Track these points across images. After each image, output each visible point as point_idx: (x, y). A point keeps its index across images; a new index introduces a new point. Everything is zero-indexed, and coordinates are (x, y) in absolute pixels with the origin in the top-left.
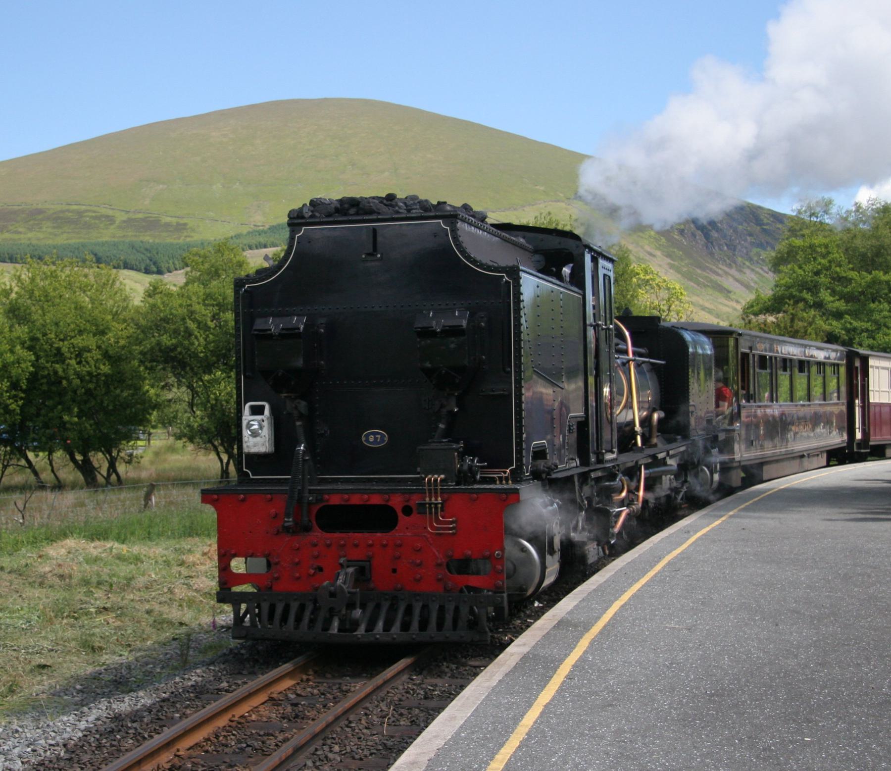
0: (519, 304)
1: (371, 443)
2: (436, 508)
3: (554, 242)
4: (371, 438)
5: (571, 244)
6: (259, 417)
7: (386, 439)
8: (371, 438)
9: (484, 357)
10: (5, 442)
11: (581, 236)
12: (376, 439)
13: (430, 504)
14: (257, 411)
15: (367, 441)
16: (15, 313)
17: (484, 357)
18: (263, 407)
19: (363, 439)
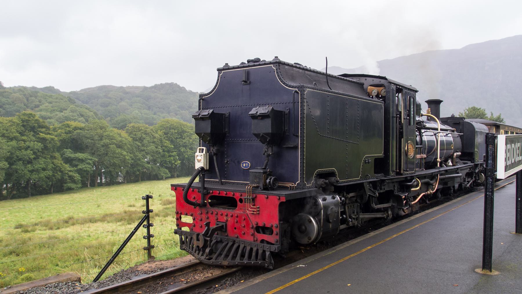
7: (250, 165)
12: (246, 165)
13: (248, 199)
15: (243, 166)
18: (203, 150)
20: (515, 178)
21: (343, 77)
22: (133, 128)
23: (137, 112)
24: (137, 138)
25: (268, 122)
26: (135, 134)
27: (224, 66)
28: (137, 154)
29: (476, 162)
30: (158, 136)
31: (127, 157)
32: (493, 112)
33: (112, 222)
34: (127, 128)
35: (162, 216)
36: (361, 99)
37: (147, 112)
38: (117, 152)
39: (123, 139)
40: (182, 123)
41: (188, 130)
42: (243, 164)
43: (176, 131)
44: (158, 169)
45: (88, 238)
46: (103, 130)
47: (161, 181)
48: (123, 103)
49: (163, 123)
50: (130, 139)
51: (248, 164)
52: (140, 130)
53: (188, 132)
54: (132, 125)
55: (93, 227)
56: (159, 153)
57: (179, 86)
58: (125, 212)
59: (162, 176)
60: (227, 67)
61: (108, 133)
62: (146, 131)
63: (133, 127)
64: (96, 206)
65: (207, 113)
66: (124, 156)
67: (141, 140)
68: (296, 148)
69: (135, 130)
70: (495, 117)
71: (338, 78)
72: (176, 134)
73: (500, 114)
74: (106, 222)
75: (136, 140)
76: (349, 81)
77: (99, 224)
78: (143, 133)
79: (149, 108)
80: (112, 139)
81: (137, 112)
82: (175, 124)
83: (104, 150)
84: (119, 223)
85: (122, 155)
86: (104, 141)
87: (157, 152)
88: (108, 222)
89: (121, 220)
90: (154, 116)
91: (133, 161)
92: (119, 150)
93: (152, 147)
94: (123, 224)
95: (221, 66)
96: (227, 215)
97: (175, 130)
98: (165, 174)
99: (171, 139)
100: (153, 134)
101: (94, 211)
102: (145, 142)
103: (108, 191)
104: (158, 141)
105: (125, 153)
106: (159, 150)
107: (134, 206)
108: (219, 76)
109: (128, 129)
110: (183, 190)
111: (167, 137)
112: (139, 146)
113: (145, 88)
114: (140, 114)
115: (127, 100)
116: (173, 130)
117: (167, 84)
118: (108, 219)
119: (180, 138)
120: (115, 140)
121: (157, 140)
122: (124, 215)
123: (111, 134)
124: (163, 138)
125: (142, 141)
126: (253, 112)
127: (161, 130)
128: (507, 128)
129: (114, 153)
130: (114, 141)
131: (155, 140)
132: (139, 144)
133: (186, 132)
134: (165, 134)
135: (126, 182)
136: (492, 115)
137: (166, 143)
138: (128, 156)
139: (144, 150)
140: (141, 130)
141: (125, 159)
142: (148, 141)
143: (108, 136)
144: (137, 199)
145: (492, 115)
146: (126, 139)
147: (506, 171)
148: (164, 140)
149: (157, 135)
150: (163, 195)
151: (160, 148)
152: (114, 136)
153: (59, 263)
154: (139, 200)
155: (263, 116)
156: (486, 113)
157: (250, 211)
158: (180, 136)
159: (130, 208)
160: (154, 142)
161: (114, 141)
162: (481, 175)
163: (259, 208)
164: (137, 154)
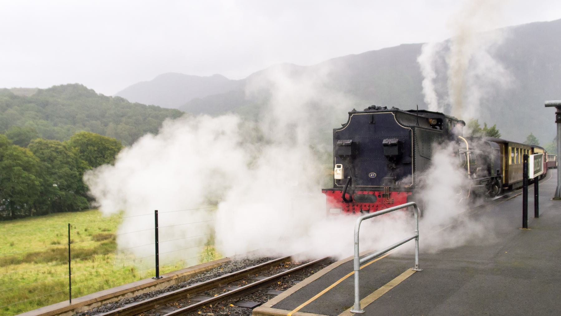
0: (414, 135)
1: (372, 177)
2: (387, 195)
3: (439, 117)
4: (372, 175)
5: (442, 117)
6: (339, 169)
7: (376, 175)
8: (372, 175)
9: (506, 252)
10: (249, 315)
11: (443, 113)
12: (373, 175)
13: (386, 195)
14: (339, 167)
15: (370, 176)
16: (2, 280)
17: (506, 252)
18: (340, 166)
19: (369, 175)
20: (522, 191)
21: (410, 113)
22: (40, 145)
23: (31, 122)
24: (46, 158)
25: (396, 148)
26: (42, 152)
27: (352, 111)
28: (48, 177)
29: (493, 176)
30: (73, 155)
31: (37, 183)
32: (487, 123)
33: (40, 262)
34: (30, 144)
35: (101, 253)
36: (429, 129)
37: (45, 122)
38: (23, 175)
39: (30, 159)
40: (103, 138)
41: (111, 147)
42: (370, 174)
43: (96, 149)
44: (74, 197)
45: (22, 280)
46: (4, 147)
47: (78, 213)
48: (10, 111)
49: (78, 138)
50: (38, 160)
51: (375, 175)
52: (48, 148)
53: (112, 149)
54: (38, 140)
55: (22, 268)
56: (76, 176)
57: (85, 89)
58: (53, 250)
59: (79, 206)
60: (354, 112)
61: (11, 151)
62: (57, 148)
63: (40, 143)
64: (9, 245)
65: (349, 143)
66: (33, 181)
67: (51, 159)
68: (411, 163)
69: (43, 148)
70: (489, 129)
71: (405, 113)
72: (96, 152)
73: (495, 125)
74: (33, 263)
75: (44, 161)
76: (412, 115)
77: (25, 266)
78: (53, 151)
79: (47, 117)
80: (15, 160)
81: (31, 122)
82: (94, 139)
83: (5, 174)
84: (50, 264)
85: (30, 179)
86: (6, 162)
87: (71, 175)
88: (36, 263)
89: (51, 260)
90: (56, 128)
91: (42, 188)
92: (25, 174)
93: (66, 169)
94: (57, 265)
95: (351, 111)
96: (369, 206)
97: (94, 146)
98: (82, 203)
99: (88, 158)
100: (67, 152)
101: (10, 251)
102: (57, 162)
103: (14, 226)
104: (73, 162)
105: (33, 177)
106: (75, 172)
107: (59, 243)
108: (349, 118)
109: (32, 146)
110: (341, 192)
111: (84, 156)
112: (48, 168)
113: (40, 91)
114: (36, 126)
115: (16, 107)
116: (92, 147)
117: (69, 86)
118: (35, 258)
119: (100, 157)
120: (21, 160)
121: (71, 160)
122: (52, 253)
123: (15, 153)
124: (78, 157)
125: (52, 161)
126: (385, 142)
127: (75, 147)
128: (513, 145)
129: (20, 176)
130: (18, 161)
131: (69, 160)
132: (49, 165)
133: (108, 149)
134: (82, 151)
135: (32, 215)
136: (486, 126)
137: (83, 163)
138: (37, 181)
139: (55, 173)
140: (51, 147)
141: (34, 184)
142: (61, 161)
143: (11, 155)
144: (59, 235)
145: (486, 126)
146: (34, 159)
147: (534, 174)
148: (80, 160)
149: (70, 154)
150: (89, 229)
151: (76, 170)
152: (19, 155)
153: (10, 307)
154: (62, 236)
155: (393, 145)
156: (479, 124)
157: (387, 202)
158: (100, 155)
159: (54, 245)
160: (68, 163)
161: (18, 161)
162: (495, 187)
163: (393, 200)
164: (48, 177)
